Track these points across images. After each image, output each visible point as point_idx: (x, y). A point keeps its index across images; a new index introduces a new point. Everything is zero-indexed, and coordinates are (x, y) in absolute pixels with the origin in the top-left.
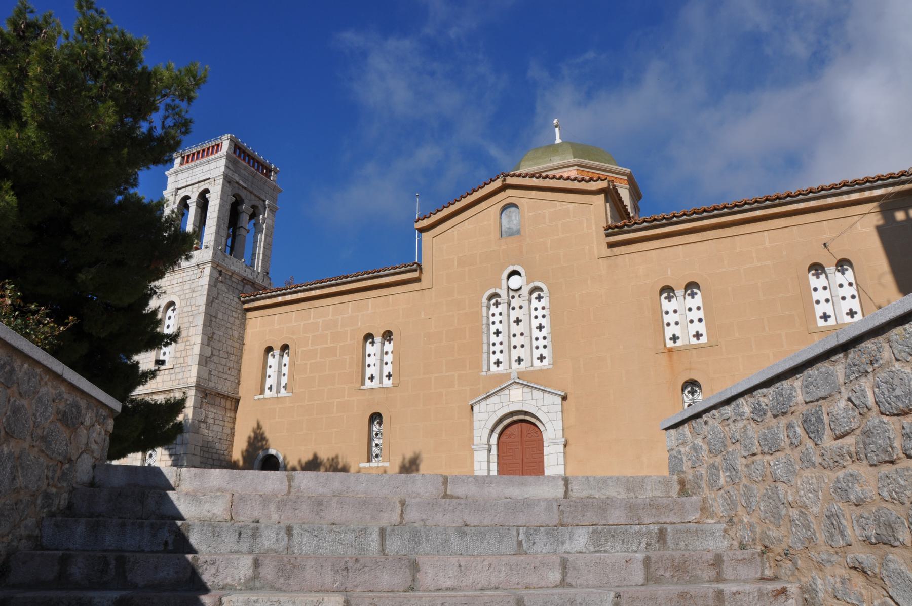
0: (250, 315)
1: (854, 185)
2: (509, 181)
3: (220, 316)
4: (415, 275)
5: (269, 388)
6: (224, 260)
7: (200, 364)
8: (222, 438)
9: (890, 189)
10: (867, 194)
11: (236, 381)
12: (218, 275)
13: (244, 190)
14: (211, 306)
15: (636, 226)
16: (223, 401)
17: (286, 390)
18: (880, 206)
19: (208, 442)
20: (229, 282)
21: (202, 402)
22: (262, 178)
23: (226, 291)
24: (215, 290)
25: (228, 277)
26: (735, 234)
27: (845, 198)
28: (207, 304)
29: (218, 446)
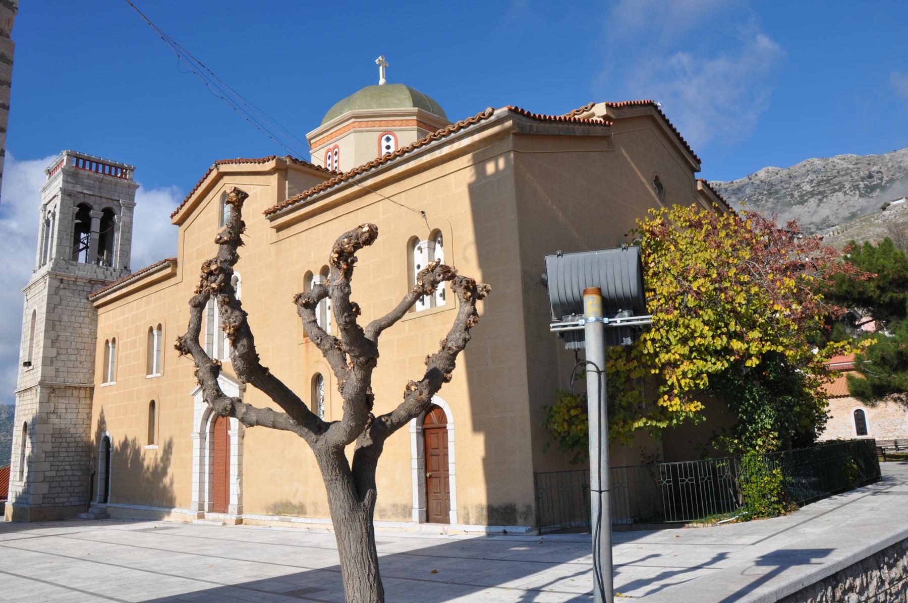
0: (100, 311)
1: (440, 138)
2: (224, 168)
3: (65, 318)
4: (168, 271)
6: (67, 268)
7: (43, 365)
8: (77, 423)
9: (476, 137)
11: (91, 372)
12: (59, 284)
13: (91, 197)
14: (54, 312)
15: (285, 209)
16: (75, 393)
17: (444, 299)
18: (474, 158)
19: (60, 429)
20: (74, 287)
21: (49, 396)
22: (111, 181)
23: (71, 295)
24: (57, 299)
25: (72, 283)
27: (438, 154)
28: (48, 312)
29: (72, 430)
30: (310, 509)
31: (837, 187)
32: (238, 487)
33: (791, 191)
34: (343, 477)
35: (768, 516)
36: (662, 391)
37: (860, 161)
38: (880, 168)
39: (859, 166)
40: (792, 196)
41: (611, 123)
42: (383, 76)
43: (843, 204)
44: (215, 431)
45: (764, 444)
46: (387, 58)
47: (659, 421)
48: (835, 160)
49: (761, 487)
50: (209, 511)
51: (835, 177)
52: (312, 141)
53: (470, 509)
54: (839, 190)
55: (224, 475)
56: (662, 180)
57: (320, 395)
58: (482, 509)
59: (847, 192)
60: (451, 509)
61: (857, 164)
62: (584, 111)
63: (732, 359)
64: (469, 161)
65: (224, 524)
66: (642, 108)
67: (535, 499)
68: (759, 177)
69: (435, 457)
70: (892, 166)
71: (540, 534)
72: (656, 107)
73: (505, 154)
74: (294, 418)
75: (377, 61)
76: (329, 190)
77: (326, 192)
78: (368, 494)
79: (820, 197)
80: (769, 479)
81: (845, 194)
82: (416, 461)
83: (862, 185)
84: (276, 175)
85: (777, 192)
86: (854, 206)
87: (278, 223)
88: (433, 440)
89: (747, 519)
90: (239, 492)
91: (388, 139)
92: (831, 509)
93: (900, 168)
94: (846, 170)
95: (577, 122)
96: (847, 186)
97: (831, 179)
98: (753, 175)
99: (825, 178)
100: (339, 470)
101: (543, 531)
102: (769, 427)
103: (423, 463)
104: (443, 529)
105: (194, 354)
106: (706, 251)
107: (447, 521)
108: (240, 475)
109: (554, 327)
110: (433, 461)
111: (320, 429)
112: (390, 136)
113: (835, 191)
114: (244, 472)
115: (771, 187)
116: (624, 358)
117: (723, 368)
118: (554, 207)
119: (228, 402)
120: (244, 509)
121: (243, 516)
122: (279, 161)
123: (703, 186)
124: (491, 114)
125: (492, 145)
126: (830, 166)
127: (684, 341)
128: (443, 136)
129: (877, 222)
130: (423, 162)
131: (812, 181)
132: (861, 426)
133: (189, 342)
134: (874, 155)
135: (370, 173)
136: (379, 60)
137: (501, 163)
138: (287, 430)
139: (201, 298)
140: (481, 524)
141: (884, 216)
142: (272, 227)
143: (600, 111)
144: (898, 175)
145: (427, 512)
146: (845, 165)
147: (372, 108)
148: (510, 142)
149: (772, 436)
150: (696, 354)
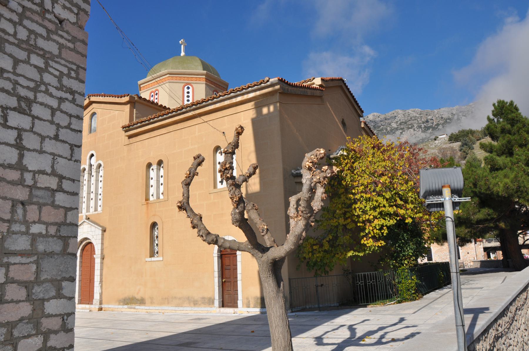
1: (237, 92)
2: (93, 99)
5: (220, 182)
9: (258, 93)
10: (246, 97)
15: (135, 126)
18: (255, 104)
26: (182, 128)
27: (234, 100)
30: (148, 301)
31: (410, 126)
32: (100, 289)
33: (386, 127)
34: (273, 275)
35: (410, 300)
36: (362, 235)
37: (422, 113)
38: (432, 117)
39: (422, 115)
40: (386, 129)
41: (324, 89)
42: (183, 51)
43: (413, 135)
44: (83, 256)
45: (408, 263)
46: (186, 41)
47: (359, 252)
48: (409, 111)
49: (407, 285)
50: (80, 302)
51: (409, 120)
52: (141, 86)
53: (250, 299)
54: (411, 128)
55: (89, 282)
56: (346, 121)
57: (154, 235)
58: (258, 299)
59: (415, 129)
60: (239, 299)
61: (420, 114)
62: (308, 81)
63: (398, 219)
64: (252, 106)
65: (90, 311)
66: (337, 81)
67: (290, 293)
68: (369, 118)
69: (227, 270)
70: (438, 117)
71: (292, 312)
72: (343, 81)
73: (274, 103)
74: (252, 245)
75: (180, 42)
76: (165, 116)
77: (163, 118)
78: (281, 284)
79: (401, 131)
80: (411, 281)
81: (414, 130)
82: (217, 272)
83: (423, 126)
84: (129, 105)
85: (379, 127)
86: (419, 137)
87: (130, 134)
88: (227, 261)
89: (399, 302)
90: (100, 292)
91: (188, 88)
92: (439, 297)
93: (442, 118)
94: (415, 117)
95: (305, 87)
96: (416, 126)
97: (407, 122)
98: (366, 117)
99: (404, 121)
100: (271, 272)
101: (293, 310)
102: (411, 254)
103: (221, 274)
104: (234, 311)
105: (188, 211)
106: (384, 162)
107: (236, 306)
108: (101, 281)
109: (427, 201)
110: (227, 272)
111: (264, 250)
112: (190, 86)
113: (409, 128)
114: (104, 280)
115: (376, 124)
116: (343, 218)
117: (394, 224)
118: (297, 133)
119: (214, 236)
120: (103, 301)
121: (103, 306)
122: (131, 97)
123: (364, 125)
124: (268, 81)
125: (267, 98)
126: (407, 114)
127: (374, 208)
128: (239, 91)
129: (432, 146)
130: (225, 104)
131: (397, 122)
132: (429, 256)
133: (185, 204)
134: (430, 110)
135: (192, 108)
136: (182, 41)
137: (272, 108)
138: (245, 251)
139: (189, 180)
140: (257, 307)
141: (435, 143)
142: (126, 136)
143: (317, 82)
144: (441, 121)
145: (223, 301)
146: (415, 115)
147: (179, 69)
148: (277, 97)
149: (412, 259)
150: (380, 216)
